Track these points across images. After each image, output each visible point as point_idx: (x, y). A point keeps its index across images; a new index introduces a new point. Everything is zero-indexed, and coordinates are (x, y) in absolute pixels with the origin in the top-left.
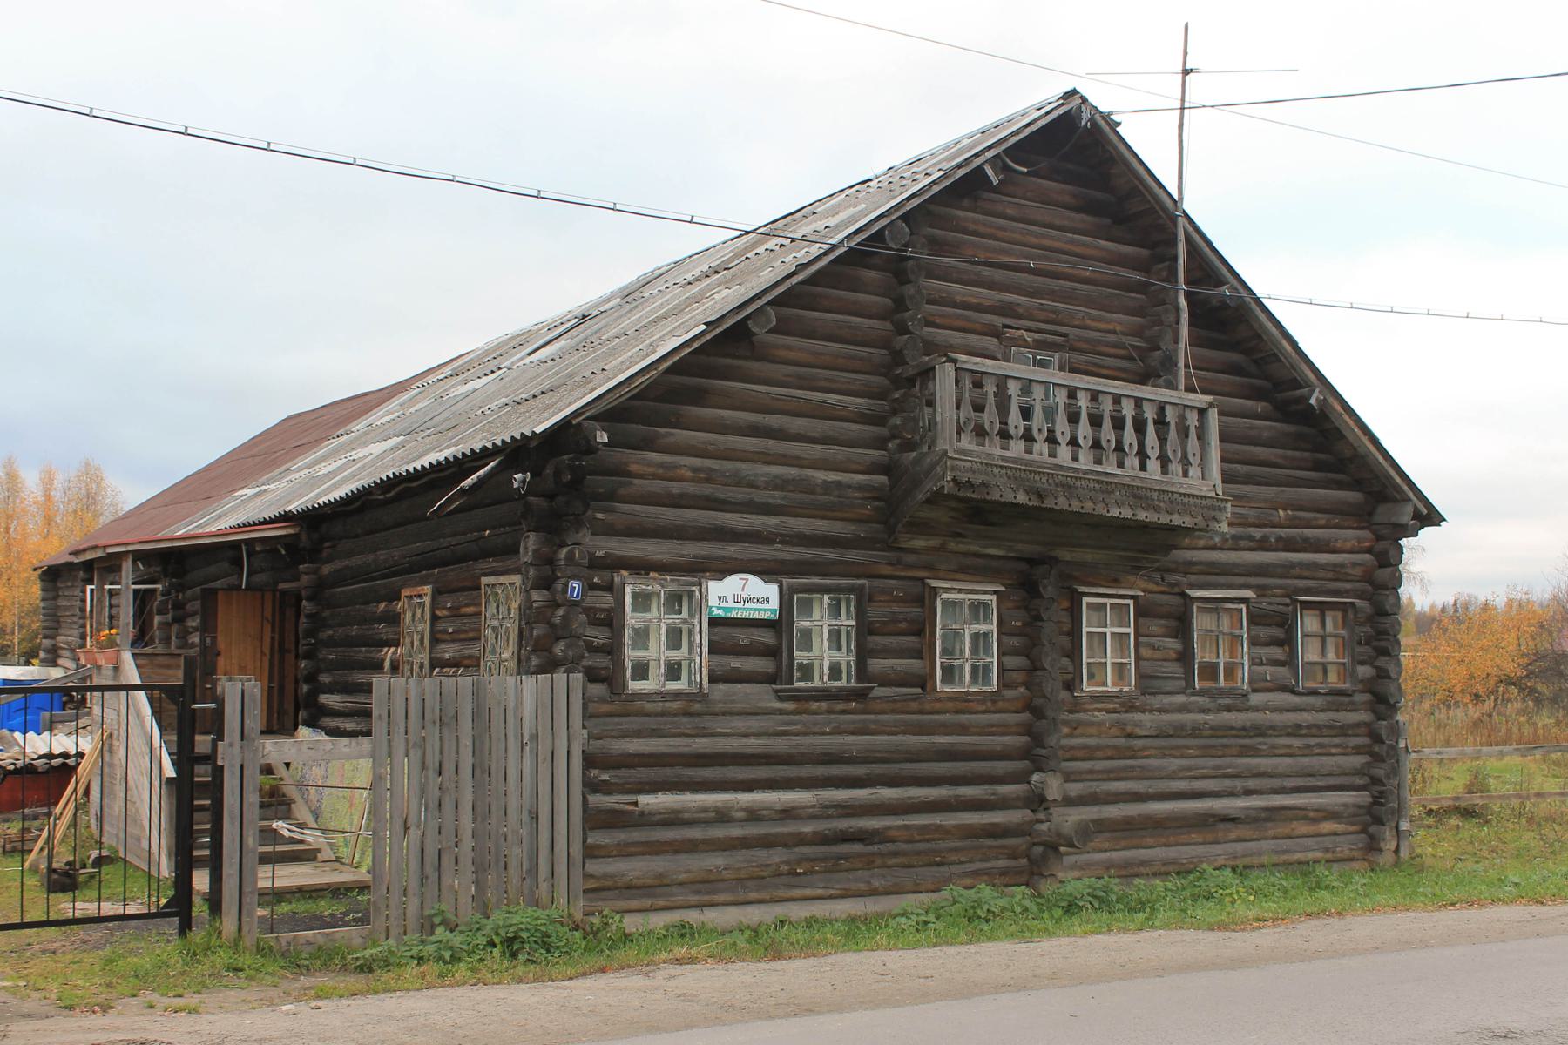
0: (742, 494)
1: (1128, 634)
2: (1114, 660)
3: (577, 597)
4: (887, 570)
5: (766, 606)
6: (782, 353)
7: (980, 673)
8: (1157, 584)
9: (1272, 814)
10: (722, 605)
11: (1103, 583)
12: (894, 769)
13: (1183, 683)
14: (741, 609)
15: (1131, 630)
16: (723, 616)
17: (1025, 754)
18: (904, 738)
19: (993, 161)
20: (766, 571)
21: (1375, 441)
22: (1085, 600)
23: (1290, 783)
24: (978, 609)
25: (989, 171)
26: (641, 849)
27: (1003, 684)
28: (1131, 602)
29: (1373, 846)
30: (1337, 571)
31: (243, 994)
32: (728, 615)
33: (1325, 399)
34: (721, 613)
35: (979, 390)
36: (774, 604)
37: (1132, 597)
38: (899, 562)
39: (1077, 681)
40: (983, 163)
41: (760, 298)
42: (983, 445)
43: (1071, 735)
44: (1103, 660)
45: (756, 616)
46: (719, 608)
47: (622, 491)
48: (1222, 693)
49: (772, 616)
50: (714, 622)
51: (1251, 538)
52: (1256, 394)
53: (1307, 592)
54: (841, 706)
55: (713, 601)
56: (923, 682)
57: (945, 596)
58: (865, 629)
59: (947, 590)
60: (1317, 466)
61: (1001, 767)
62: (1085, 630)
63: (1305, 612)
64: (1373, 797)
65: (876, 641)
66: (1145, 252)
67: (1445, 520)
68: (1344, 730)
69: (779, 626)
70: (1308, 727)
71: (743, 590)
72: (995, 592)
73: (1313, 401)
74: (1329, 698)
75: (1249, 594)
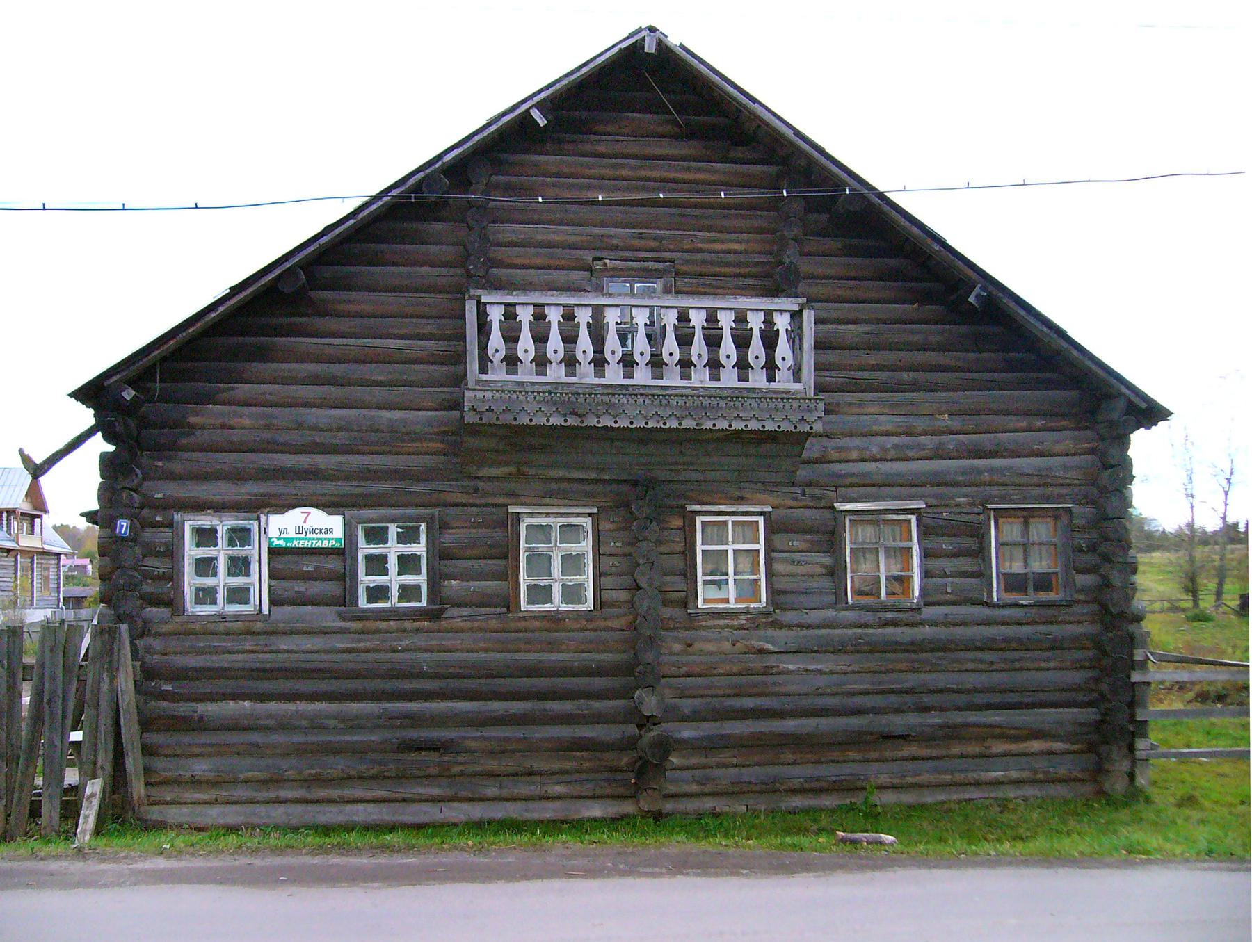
0: (307, 437)
1: (758, 551)
3: (125, 533)
4: (463, 499)
5: (328, 536)
6: (341, 307)
7: (572, 593)
8: (795, 499)
9: (953, 733)
10: (282, 536)
11: (722, 501)
12: (470, 684)
13: (832, 598)
14: (303, 539)
15: (761, 547)
16: (284, 545)
17: (627, 669)
19: (538, 106)
20: (330, 506)
21: (1062, 334)
23: (979, 699)
24: (571, 532)
25: (536, 114)
27: (600, 603)
28: (761, 519)
29: (1099, 771)
30: (1043, 480)
31: (517, 838)
32: (289, 545)
33: (990, 294)
34: (282, 543)
35: (570, 323)
36: (339, 533)
37: (761, 513)
38: (476, 491)
39: (691, 599)
40: (530, 108)
41: (286, 261)
42: (516, 373)
43: (685, 653)
44: (737, 577)
45: (319, 544)
46: (278, 539)
47: (183, 441)
48: (884, 608)
49: (338, 545)
50: (274, 552)
52: (925, 298)
53: (1003, 499)
54: (408, 625)
55: (273, 532)
56: (509, 602)
58: (439, 554)
59: (532, 515)
60: (1010, 367)
61: (599, 683)
62: (700, 548)
63: (1001, 521)
64: (1101, 714)
65: (450, 566)
66: (771, 170)
67: (1151, 414)
68: (1055, 645)
69: (344, 552)
70: (1004, 641)
71: (305, 522)
72: (590, 515)
73: (971, 299)
74: (1035, 610)
75: (920, 505)
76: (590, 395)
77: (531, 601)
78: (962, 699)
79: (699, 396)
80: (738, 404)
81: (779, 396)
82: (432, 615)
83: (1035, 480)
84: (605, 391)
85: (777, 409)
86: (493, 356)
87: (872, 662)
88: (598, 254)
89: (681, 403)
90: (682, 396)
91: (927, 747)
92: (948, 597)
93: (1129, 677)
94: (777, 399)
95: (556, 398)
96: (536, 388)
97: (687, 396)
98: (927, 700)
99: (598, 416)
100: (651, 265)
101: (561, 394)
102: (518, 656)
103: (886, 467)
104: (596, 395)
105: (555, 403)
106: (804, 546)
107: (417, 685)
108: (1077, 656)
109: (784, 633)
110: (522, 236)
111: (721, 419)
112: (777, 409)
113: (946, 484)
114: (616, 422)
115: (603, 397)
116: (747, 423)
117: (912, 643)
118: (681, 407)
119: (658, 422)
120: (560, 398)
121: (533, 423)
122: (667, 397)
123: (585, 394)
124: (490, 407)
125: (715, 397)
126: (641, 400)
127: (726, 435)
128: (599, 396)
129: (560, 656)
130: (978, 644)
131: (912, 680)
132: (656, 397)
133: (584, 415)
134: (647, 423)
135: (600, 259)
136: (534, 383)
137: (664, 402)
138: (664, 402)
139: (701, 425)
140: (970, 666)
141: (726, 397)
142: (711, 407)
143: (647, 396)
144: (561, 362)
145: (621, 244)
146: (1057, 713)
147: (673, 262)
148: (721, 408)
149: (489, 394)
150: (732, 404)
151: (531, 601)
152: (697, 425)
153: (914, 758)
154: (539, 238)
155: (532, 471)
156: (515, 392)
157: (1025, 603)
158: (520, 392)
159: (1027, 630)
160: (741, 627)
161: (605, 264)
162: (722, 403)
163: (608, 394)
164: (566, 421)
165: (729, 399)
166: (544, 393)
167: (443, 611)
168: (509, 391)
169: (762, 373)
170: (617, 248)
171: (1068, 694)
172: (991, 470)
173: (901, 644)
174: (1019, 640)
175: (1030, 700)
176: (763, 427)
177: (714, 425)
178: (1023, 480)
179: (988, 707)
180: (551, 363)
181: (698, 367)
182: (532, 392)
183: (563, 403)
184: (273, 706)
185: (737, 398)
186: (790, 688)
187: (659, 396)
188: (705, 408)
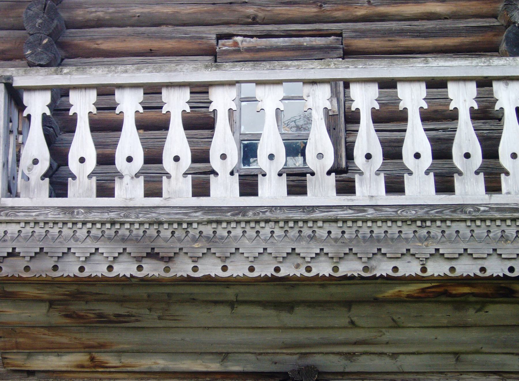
76: (180, 224)
79: (365, 221)
80: (435, 231)
81: (508, 215)
84: (206, 218)
85: (504, 238)
86: (29, 169)
88: (225, 30)
89: (336, 232)
90: (336, 221)
94: (504, 220)
95: (124, 231)
96: (92, 216)
97: (345, 221)
99: (195, 259)
100: (306, 41)
101: (132, 224)
104: (190, 224)
105: (124, 240)
110: (111, 10)
111: (408, 258)
112: (504, 238)
114: (224, 268)
115: (201, 228)
116: (453, 264)
118: (336, 240)
119: (298, 266)
120: (130, 231)
121: (85, 274)
122: (310, 224)
123: (170, 223)
124: (14, 249)
125: (394, 221)
126: (266, 231)
127: (423, 290)
128: (195, 225)
132: (291, 224)
133: (170, 259)
134: (277, 270)
135: (229, 36)
136: (89, 209)
137: (306, 232)
138: (306, 232)
139: (374, 269)
141: (414, 221)
142: (387, 238)
143: (277, 222)
144: (137, 176)
145: (261, 14)
147: (340, 35)
148: (407, 239)
149: (13, 229)
150: (424, 232)
152: (366, 269)
154: (137, 10)
155: (112, 360)
156: (55, 223)
158: (65, 223)
161: (236, 44)
162: (408, 231)
163: (210, 222)
164: (140, 268)
165: (419, 223)
166: (103, 224)
168: (46, 223)
169: (477, 181)
170: (254, 21)
176: (483, 270)
177: (395, 269)
180: (121, 177)
181: (367, 174)
182: (84, 223)
183: (137, 240)
185: (433, 221)
187: (296, 222)
188: (379, 240)
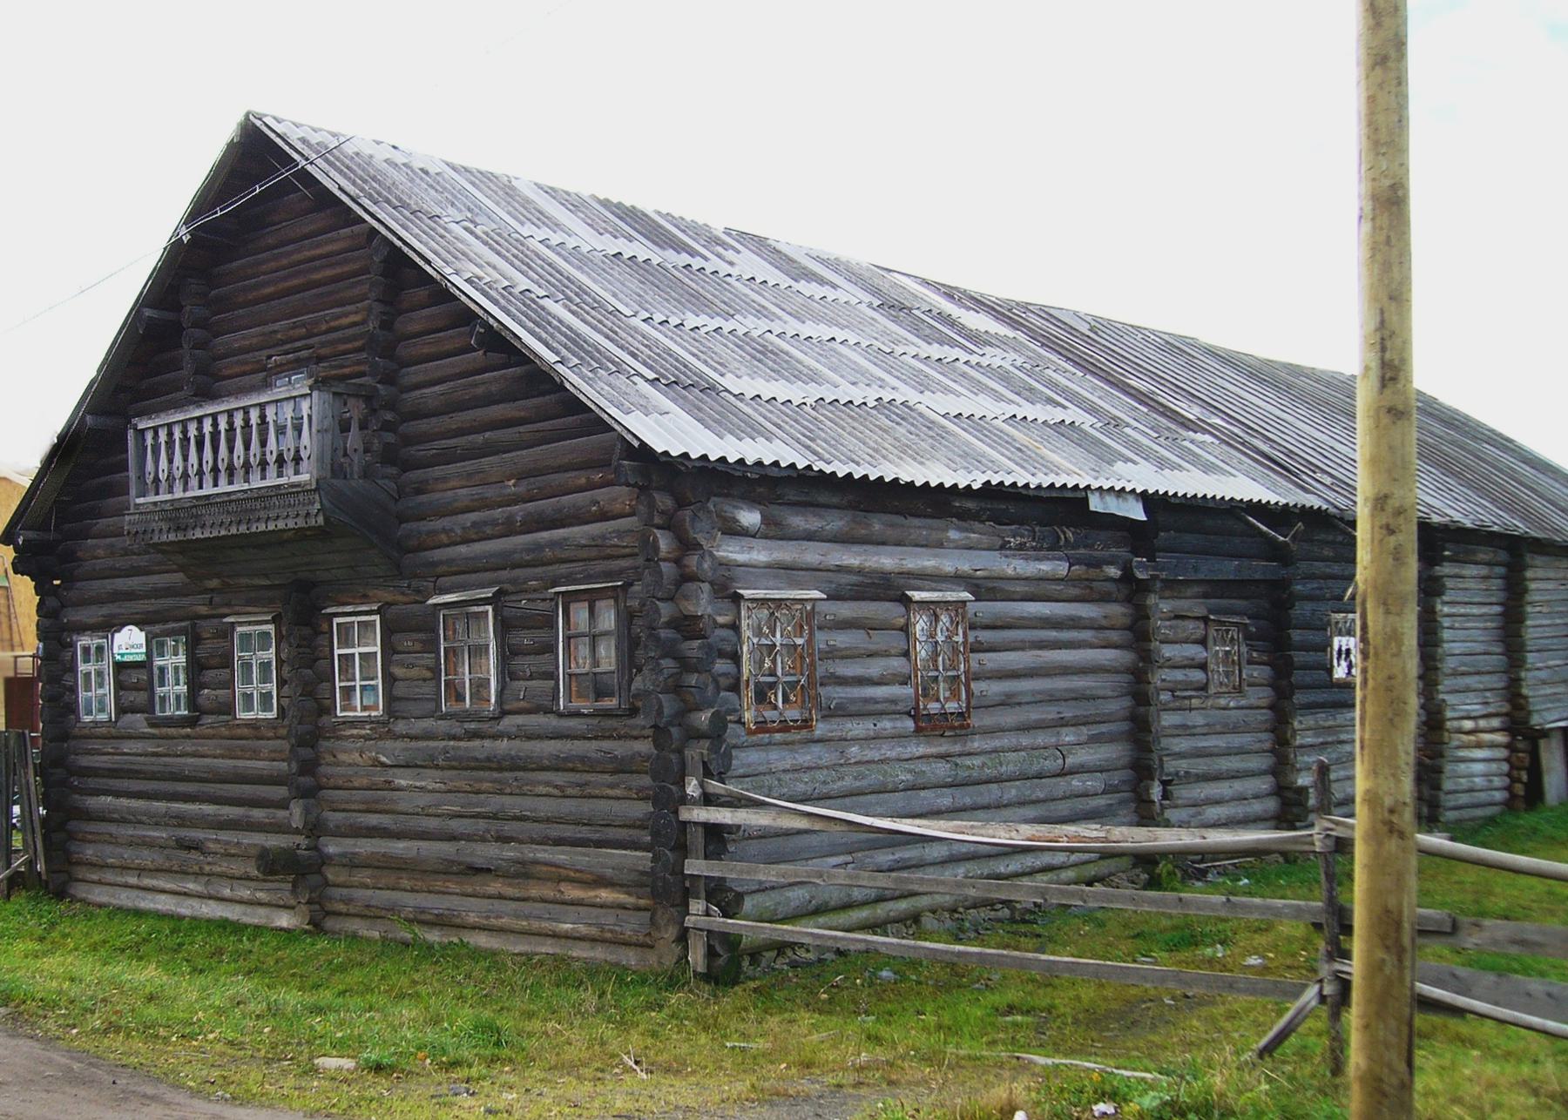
2: (343, 684)
8: (403, 594)
18: (1454, 681)
22: (336, 620)
23: (556, 831)
26: (551, 790)
28: (377, 618)
51: (494, 523)
57: (239, 629)
59: (241, 624)
68: (621, 767)
74: (595, 721)
77: (342, 711)
78: (537, 829)
82: (191, 722)
83: (594, 553)
87: (460, 780)
91: (510, 885)
92: (522, 704)
93: (676, 812)
98: (509, 828)
102: (240, 763)
103: (478, 548)
106: (418, 646)
107: (182, 787)
108: (641, 783)
109: (399, 744)
113: (515, 566)
117: (488, 759)
129: (260, 764)
130: (546, 762)
131: (495, 803)
140: (542, 789)
146: (621, 855)
151: (342, 711)
153: (501, 897)
157: (586, 711)
159: (579, 747)
160: (367, 738)
167: (198, 718)
170: (284, 342)
171: (632, 832)
172: (553, 544)
173: (477, 759)
174: (583, 759)
175: (596, 836)
178: (584, 554)
179: (559, 842)
184: (124, 802)
186: (402, 806)
